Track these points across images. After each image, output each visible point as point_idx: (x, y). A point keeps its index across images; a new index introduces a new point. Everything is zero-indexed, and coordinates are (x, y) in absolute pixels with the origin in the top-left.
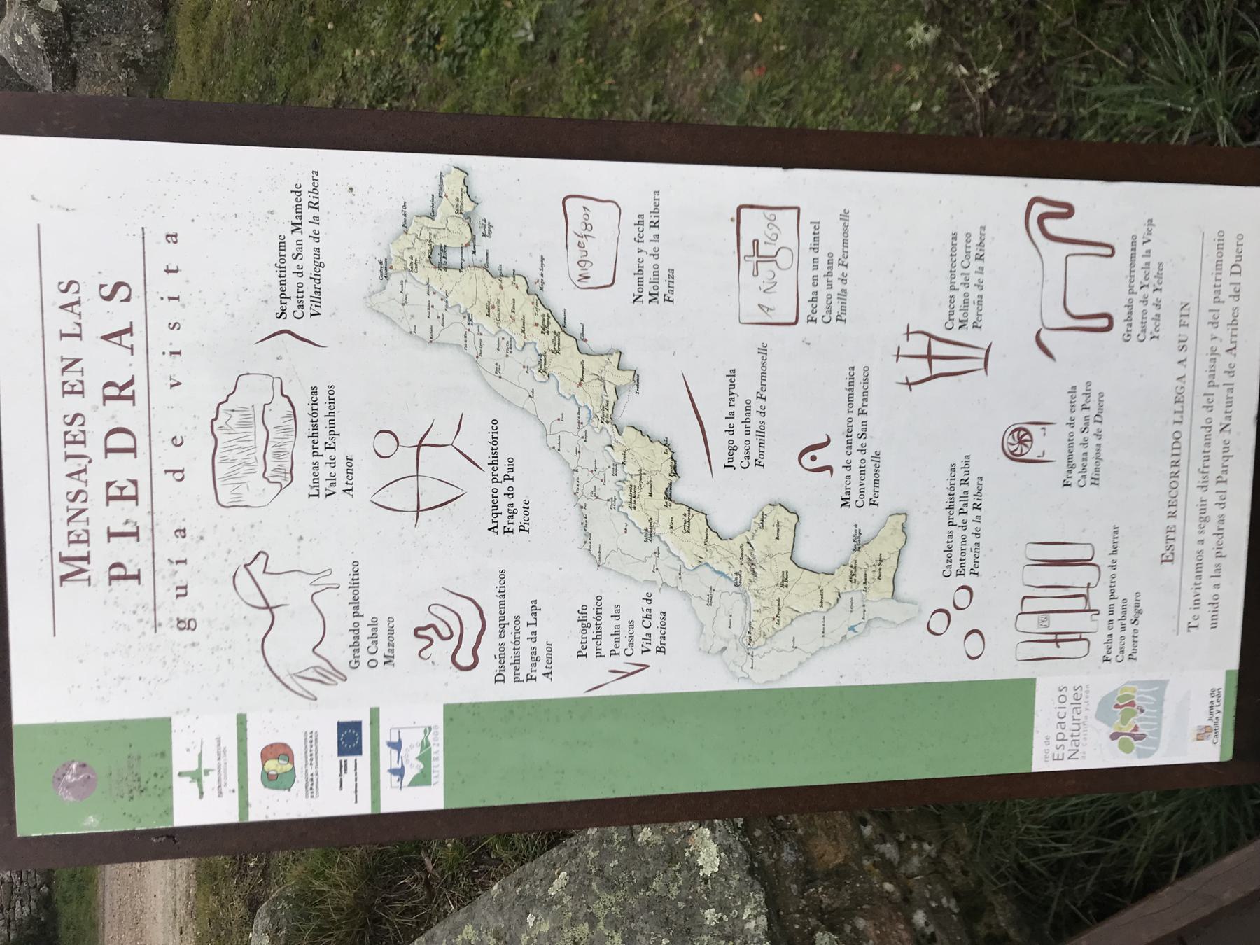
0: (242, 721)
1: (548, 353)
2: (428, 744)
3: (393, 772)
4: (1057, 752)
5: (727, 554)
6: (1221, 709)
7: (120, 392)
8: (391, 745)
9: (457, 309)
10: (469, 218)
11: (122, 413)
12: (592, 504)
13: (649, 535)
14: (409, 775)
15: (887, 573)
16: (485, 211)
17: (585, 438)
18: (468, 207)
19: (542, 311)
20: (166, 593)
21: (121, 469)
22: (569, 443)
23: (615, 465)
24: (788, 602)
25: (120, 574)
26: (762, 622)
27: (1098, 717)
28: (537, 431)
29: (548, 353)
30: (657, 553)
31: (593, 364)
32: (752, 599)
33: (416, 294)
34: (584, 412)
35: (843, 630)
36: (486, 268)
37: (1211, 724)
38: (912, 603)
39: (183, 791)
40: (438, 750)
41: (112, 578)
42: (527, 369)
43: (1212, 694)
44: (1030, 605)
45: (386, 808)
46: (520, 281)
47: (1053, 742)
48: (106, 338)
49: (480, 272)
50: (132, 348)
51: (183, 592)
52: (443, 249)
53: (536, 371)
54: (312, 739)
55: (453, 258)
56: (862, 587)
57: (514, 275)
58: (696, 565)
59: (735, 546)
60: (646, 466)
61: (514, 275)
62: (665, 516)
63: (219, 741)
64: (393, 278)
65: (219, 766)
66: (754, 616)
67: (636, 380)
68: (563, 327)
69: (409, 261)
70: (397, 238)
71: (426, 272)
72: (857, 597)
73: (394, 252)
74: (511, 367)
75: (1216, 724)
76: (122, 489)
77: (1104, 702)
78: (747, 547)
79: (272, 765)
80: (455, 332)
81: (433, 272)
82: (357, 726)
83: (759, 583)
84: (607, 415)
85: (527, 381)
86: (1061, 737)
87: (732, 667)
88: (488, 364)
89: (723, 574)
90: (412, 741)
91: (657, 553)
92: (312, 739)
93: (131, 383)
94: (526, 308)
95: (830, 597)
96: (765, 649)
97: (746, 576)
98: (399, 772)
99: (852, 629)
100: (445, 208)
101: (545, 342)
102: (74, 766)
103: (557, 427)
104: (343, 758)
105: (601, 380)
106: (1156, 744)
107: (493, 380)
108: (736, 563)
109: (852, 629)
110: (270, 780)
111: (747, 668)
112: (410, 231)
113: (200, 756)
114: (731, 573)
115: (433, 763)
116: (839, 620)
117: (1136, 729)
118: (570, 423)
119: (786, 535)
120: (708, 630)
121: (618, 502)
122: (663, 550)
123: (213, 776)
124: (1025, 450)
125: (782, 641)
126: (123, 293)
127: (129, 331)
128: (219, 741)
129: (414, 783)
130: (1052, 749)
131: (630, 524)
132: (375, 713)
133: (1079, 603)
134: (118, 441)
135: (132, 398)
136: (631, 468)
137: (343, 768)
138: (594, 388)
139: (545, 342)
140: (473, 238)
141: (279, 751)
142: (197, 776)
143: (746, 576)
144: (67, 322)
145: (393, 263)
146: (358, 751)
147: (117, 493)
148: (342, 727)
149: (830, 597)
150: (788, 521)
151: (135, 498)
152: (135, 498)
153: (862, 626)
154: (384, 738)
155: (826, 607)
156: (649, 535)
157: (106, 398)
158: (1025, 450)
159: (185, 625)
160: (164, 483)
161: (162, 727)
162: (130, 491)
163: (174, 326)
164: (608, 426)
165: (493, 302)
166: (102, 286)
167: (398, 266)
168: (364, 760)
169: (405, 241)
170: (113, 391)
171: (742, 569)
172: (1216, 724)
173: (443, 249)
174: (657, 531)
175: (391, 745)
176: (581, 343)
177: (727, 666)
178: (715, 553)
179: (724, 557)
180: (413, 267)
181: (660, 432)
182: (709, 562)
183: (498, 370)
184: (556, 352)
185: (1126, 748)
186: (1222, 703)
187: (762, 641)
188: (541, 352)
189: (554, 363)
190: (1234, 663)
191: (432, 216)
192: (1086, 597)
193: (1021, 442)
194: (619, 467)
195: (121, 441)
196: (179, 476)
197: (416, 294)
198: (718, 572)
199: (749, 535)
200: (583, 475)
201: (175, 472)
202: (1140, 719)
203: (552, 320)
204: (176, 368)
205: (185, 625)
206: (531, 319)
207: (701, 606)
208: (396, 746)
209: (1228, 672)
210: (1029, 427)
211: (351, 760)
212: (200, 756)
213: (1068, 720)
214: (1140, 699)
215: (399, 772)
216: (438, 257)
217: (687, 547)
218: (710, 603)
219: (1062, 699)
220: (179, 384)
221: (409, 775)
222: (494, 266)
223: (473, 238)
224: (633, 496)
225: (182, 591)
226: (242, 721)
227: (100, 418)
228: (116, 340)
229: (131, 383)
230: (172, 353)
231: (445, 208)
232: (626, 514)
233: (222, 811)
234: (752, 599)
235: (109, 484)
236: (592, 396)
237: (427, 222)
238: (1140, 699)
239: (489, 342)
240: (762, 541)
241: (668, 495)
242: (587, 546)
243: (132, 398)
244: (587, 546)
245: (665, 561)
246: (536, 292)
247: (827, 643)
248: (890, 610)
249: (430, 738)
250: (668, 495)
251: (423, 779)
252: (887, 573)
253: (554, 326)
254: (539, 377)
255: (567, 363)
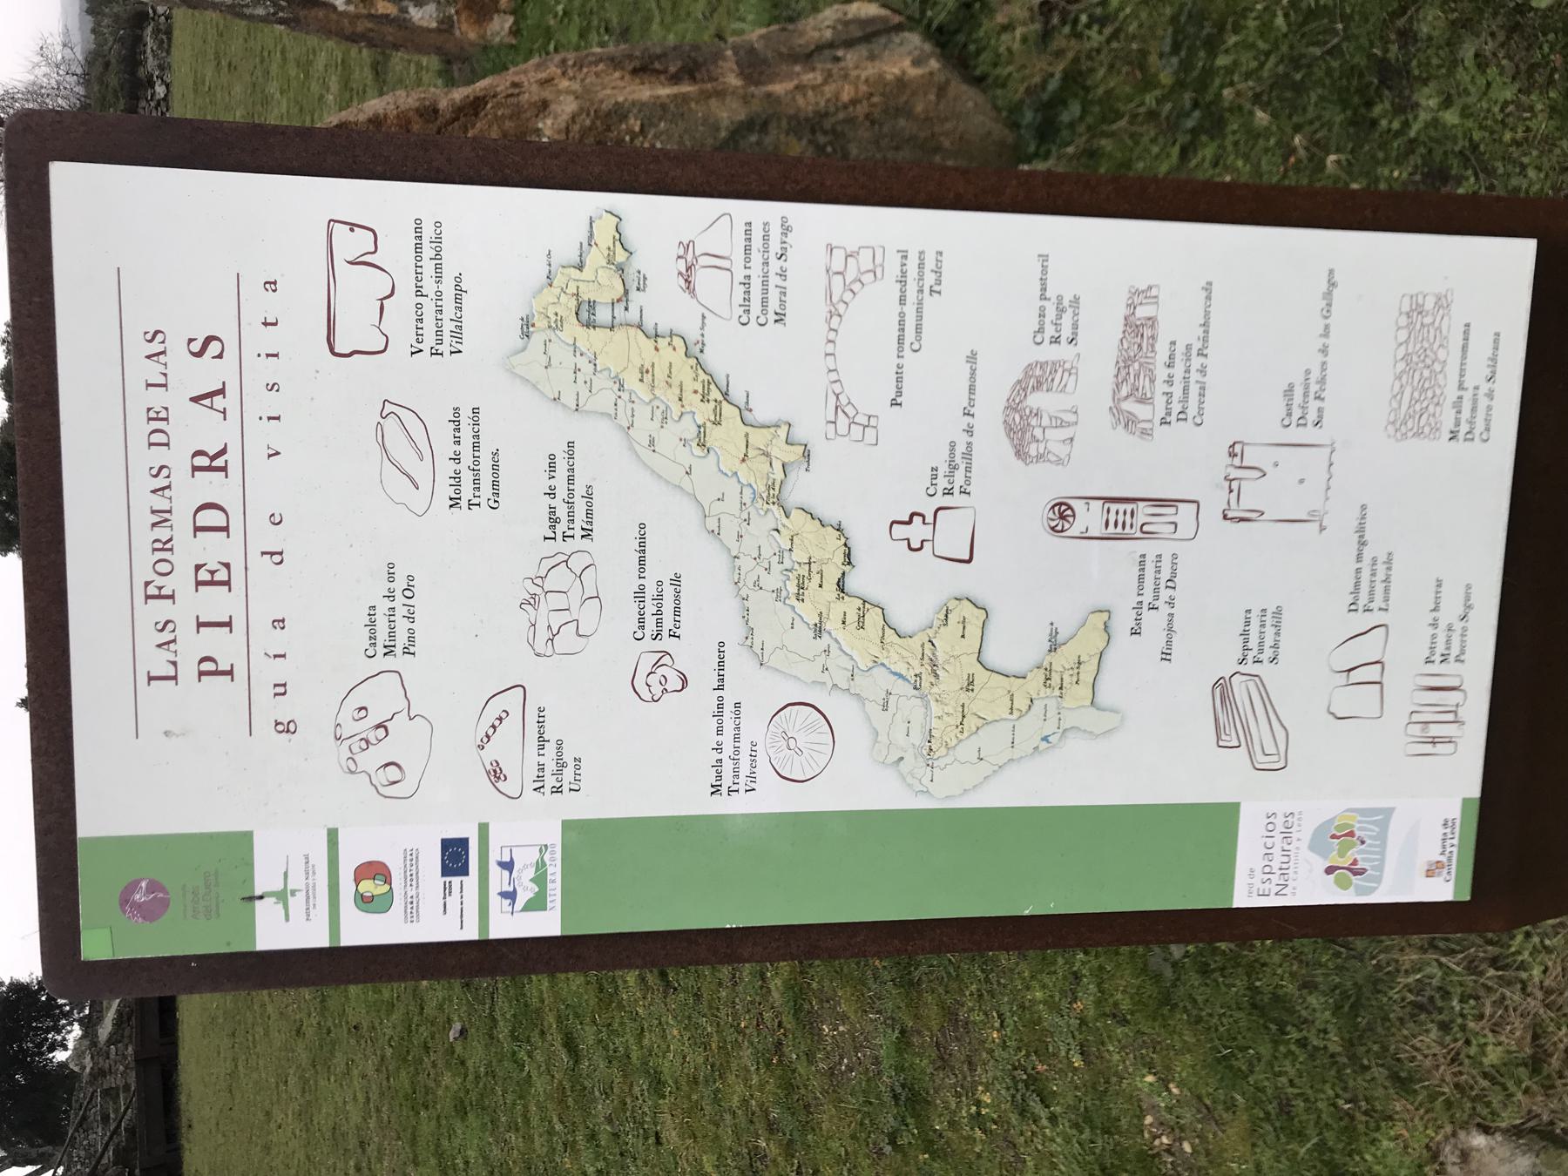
0: (333, 836)
1: (709, 424)
2: (544, 864)
3: (504, 895)
4: (1262, 887)
5: (905, 653)
6: (1455, 842)
7: (211, 462)
8: (503, 865)
9: (606, 373)
10: (621, 269)
11: (210, 487)
12: (755, 596)
13: (819, 630)
14: (522, 899)
15: (1087, 677)
16: (639, 263)
17: (748, 521)
18: (621, 256)
19: (702, 376)
20: (263, 694)
21: (212, 549)
22: (730, 529)
23: (782, 552)
24: (973, 707)
25: (210, 669)
26: (944, 728)
27: (1312, 848)
28: (691, 513)
29: (709, 424)
30: (827, 651)
31: (759, 438)
32: (933, 703)
33: (560, 353)
34: (747, 492)
35: (1036, 741)
36: (640, 327)
37: (1443, 859)
38: (1112, 711)
39: (265, 912)
40: (555, 871)
41: (201, 674)
42: (685, 442)
43: (1445, 824)
44: (1416, 718)
45: (494, 934)
46: (677, 342)
47: (1259, 876)
48: (195, 400)
49: (632, 331)
50: (224, 412)
51: (281, 690)
52: (592, 305)
53: (694, 444)
54: (412, 857)
55: (603, 315)
56: (1057, 693)
57: (671, 335)
58: (871, 664)
59: (915, 643)
60: (816, 556)
61: (671, 335)
62: (838, 609)
63: (307, 857)
64: (534, 338)
65: (307, 885)
66: (935, 723)
67: (807, 455)
68: (725, 395)
69: (553, 318)
70: (540, 291)
71: (572, 329)
72: (1052, 704)
73: (537, 308)
74: (668, 439)
75: (1450, 859)
76: (212, 573)
77: (1318, 832)
78: (928, 645)
79: (367, 887)
80: (604, 398)
81: (581, 332)
82: (463, 843)
83: (942, 687)
84: (775, 496)
85: (685, 456)
86: (1267, 870)
87: (909, 780)
88: (640, 435)
89: (901, 676)
90: (525, 861)
91: (827, 651)
92: (412, 857)
93: (223, 452)
94: (684, 372)
95: (1021, 703)
96: (949, 760)
97: (927, 678)
98: (511, 896)
99: (1045, 739)
100: (595, 258)
101: (704, 412)
102: (143, 884)
103: (718, 508)
104: (448, 879)
105: (767, 455)
106: (1378, 880)
107: (645, 454)
108: (916, 663)
109: (1045, 739)
110: (365, 902)
111: (926, 781)
112: (555, 283)
113: (286, 874)
114: (910, 675)
115: (550, 886)
116: (1030, 728)
117: (1355, 862)
118: (732, 505)
119: (973, 631)
120: (883, 738)
121: (784, 594)
122: (834, 646)
123: (301, 896)
124: (1067, 526)
125: (967, 751)
126: (214, 348)
127: (221, 392)
128: (307, 857)
129: (527, 908)
130: (1257, 881)
131: (797, 619)
132: (484, 829)
133: (1450, 717)
134: (211, 518)
135: (224, 469)
136: (800, 555)
137: (447, 890)
138: (761, 465)
139: (704, 412)
140: (626, 292)
141: (374, 870)
142: (282, 896)
143: (927, 678)
144: (153, 372)
145: (535, 321)
146: (464, 871)
147: (207, 577)
148: (447, 844)
149: (1021, 703)
150: (975, 617)
151: (227, 583)
152: (227, 583)
153: (1057, 736)
154: (494, 856)
155: (1016, 714)
156: (819, 630)
157: (195, 469)
158: (1067, 526)
159: (286, 728)
160: (260, 565)
161: (243, 841)
162: (222, 575)
163: (272, 387)
164: (774, 508)
165: (647, 366)
166: (191, 341)
167: (541, 323)
168: (471, 881)
169: (549, 295)
170: (202, 461)
171: (922, 670)
172: (1450, 859)
173: (592, 305)
174: (828, 626)
175: (503, 865)
176: (746, 413)
177: (904, 779)
178: (892, 654)
179: (902, 657)
180: (558, 325)
181: (831, 515)
182: (886, 662)
183: (652, 442)
184: (717, 423)
185: (1343, 885)
186: (1457, 835)
187: (943, 751)
188: (700, 422)
189: (715, 436)
190: (1474, 790)
191: (580, 267)
192: (1455, 712)
193: (1062, 517)
194: (786, 554)
195: (212, 519)
196: (277, 558)
197: (560, 353)
198: (895, 674)
199: (931, 632)
200: (746, 563)
201: (272, 554)
202: (1359, 852)
203: (712, 387)
204: (274, 435)
205: (286, 728)
206: (690, 386)
207: (874, 709)
208: (508, 866)
209: (1466, 801)
210: (1070, 502)
211: (456, 880)
212: (286, 874)
213: (1277, 851)
214: (1360, 829)
215: (511, 896)
216: (586, 314)
217: (859, 646)
218: (885, 707)
219: (1270, 827)
220: (277, 453)
221: (522, 899)
222: (649, 325)
223: (626, 292)
224: (801, 587)
225: (281, 689)
226: (333, 836)
227: (190, 491)
228: (207, 402)
229: (223, 452)
230: (269, 418)
231: (595, 258)
232: (793, 608)
233: (315, 937)
234: (933, 703)
235: (198, 567)
236: (755, 474)
237: (575, 273)
238: (1360, 829)
239: (643, 412)
240: (946, 642)
241: (841, 586)
242: (749, 642)
243: (224, 469)
244: (749, 642)
245: (837, 661)
246: (694, 352)
247: (1016, 754)
248: (1089, 718)
249: (547, 858)
250: (841, 586)
251: (537, 904)
252: (1087, 677)
253: (715, 394)
254: (698, 451)
255: (728, 436)
